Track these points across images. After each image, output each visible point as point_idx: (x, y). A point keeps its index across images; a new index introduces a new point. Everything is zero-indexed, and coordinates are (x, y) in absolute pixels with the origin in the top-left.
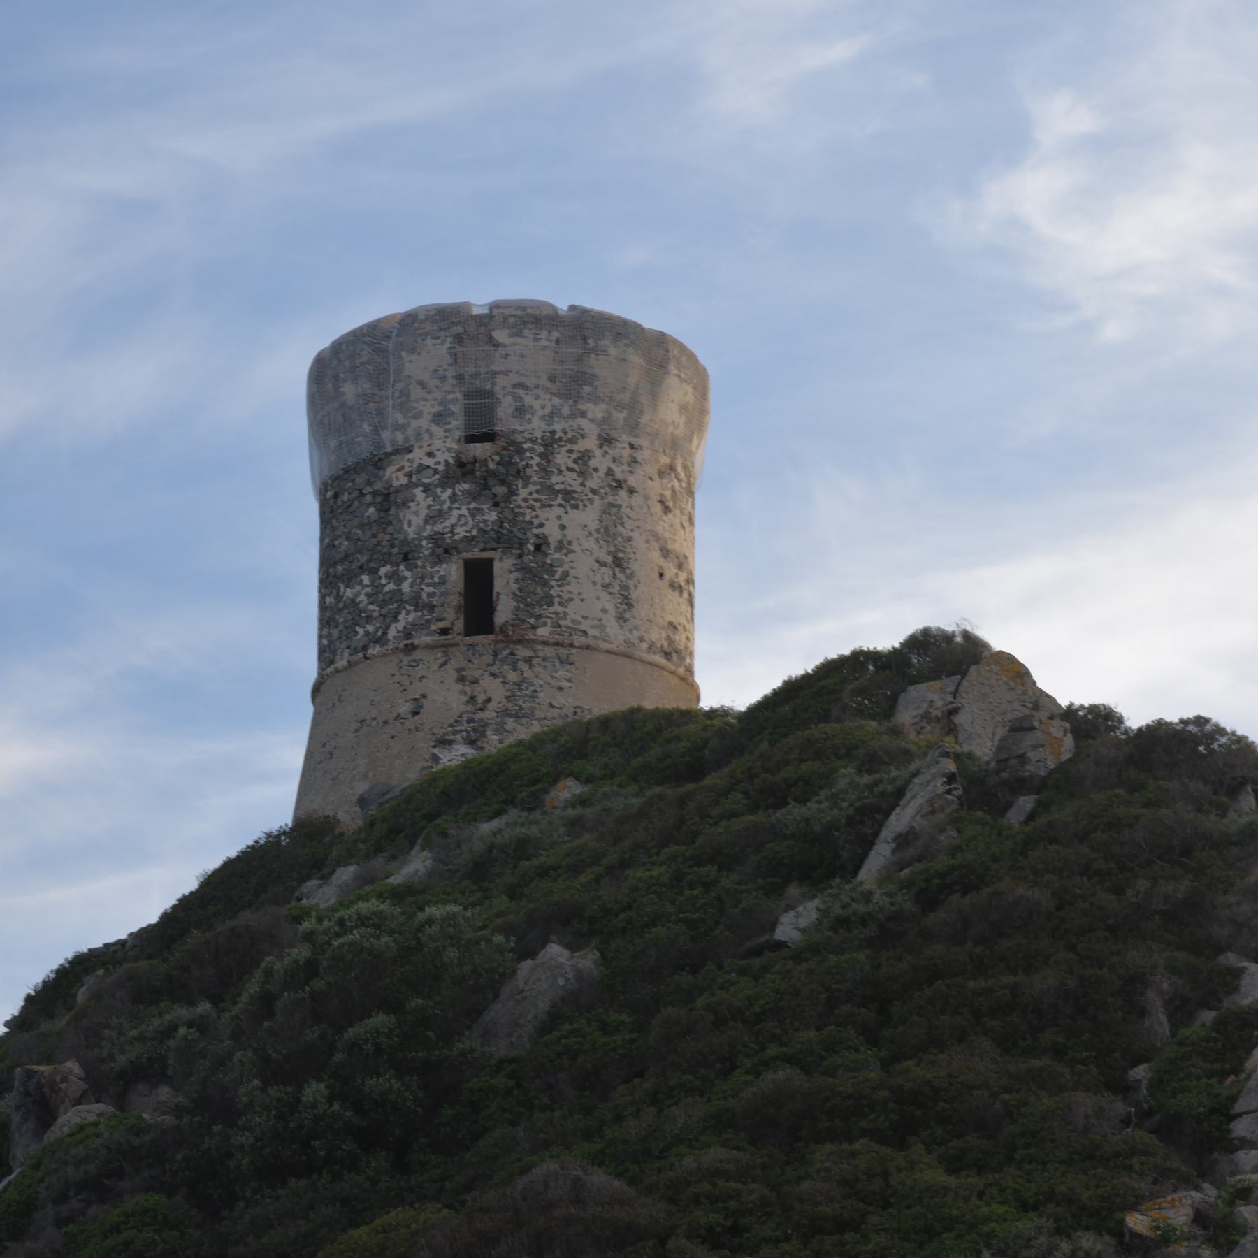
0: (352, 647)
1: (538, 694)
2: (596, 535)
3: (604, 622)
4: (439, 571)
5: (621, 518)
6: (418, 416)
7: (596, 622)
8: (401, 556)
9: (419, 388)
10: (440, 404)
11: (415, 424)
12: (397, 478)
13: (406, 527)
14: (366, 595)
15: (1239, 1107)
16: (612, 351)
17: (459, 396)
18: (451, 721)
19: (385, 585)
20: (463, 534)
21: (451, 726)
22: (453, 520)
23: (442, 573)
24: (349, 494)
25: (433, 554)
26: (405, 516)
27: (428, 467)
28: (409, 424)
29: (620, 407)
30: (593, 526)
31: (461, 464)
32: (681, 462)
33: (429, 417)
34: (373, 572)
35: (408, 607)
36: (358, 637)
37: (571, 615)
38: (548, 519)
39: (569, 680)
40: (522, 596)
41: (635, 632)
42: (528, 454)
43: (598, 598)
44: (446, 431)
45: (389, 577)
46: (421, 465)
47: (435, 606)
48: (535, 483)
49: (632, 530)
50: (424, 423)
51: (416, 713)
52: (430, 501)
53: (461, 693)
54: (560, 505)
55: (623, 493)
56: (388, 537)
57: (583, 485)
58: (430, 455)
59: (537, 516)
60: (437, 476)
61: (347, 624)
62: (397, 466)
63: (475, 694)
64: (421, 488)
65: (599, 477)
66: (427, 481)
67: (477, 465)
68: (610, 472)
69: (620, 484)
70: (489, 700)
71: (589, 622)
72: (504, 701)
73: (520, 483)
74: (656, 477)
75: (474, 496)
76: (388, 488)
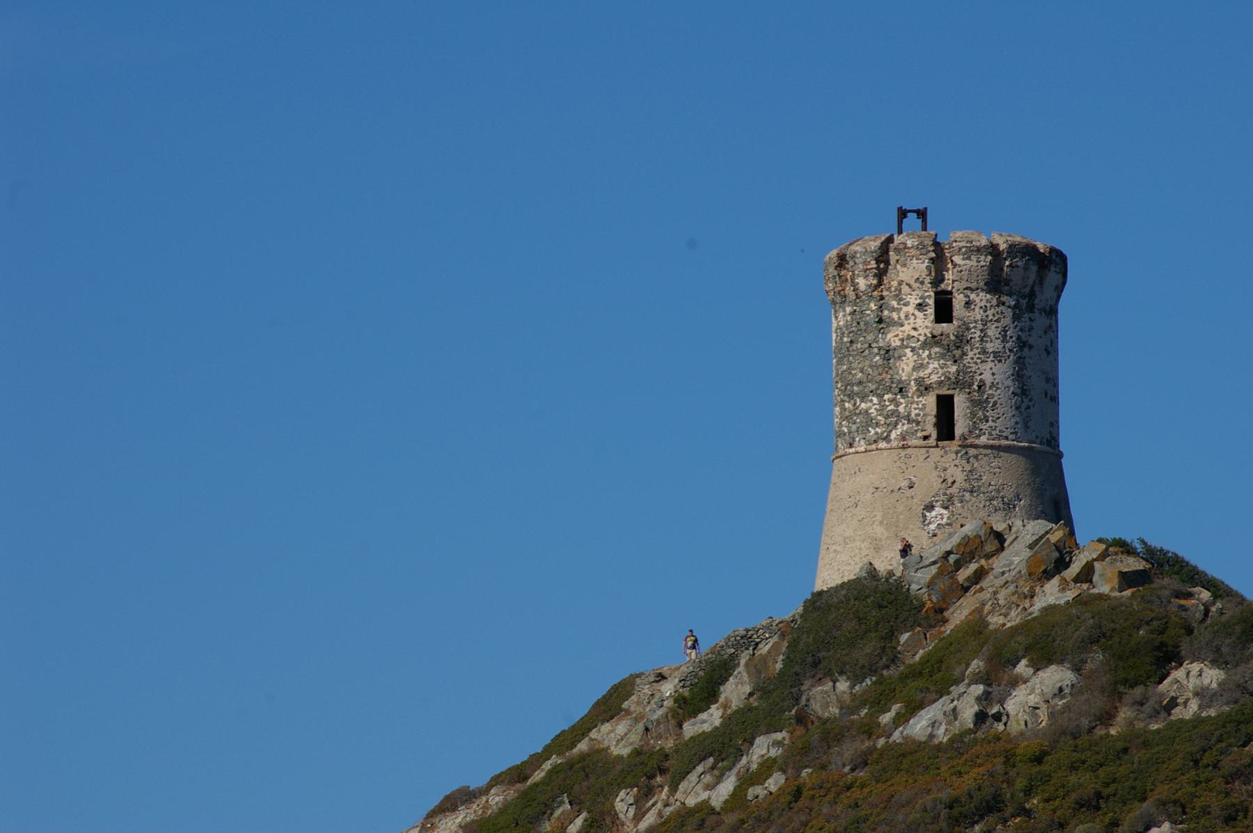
0: (867, 439)
1: (983, 478)
4: (921, 401)
5: (1025, 365)
6: (906, 304)
9: (907, 287)
10: (920, 298)
11: (905, 309)
12: (895, 342)
13: (900, 372)
14: (875, 409)
17: (932, 294)
18: (933, 494)
19: (888, 406)
20: (936, 379)
21: (934, 497)
22: (929, 371)
23: (924, 402)
24: (862, 344)
25: (918, 390)
26: (899, 365)
27: (913, 337)
28: (901, 309)
35: (903, 421)
36: (871, 434)
38: (985, 370)
42: (973, 330)
44: (924, 315)
45: (891, 401)
46: (909, 335)
47: (920, 422)
48: (977, 348)
50: (911, 309)
52: (915, 357)
53: (938, 477)
55: (1026, 350)
58: (915, 329)
60: (920, 343)
61: (862, 424)
62: (895, 334)
63: (946, 478)
64: (910, 349)
66: (913, 345)
70: (954, 482)
72: (964, 482)
75: (943, 356)
76: (889, 346)
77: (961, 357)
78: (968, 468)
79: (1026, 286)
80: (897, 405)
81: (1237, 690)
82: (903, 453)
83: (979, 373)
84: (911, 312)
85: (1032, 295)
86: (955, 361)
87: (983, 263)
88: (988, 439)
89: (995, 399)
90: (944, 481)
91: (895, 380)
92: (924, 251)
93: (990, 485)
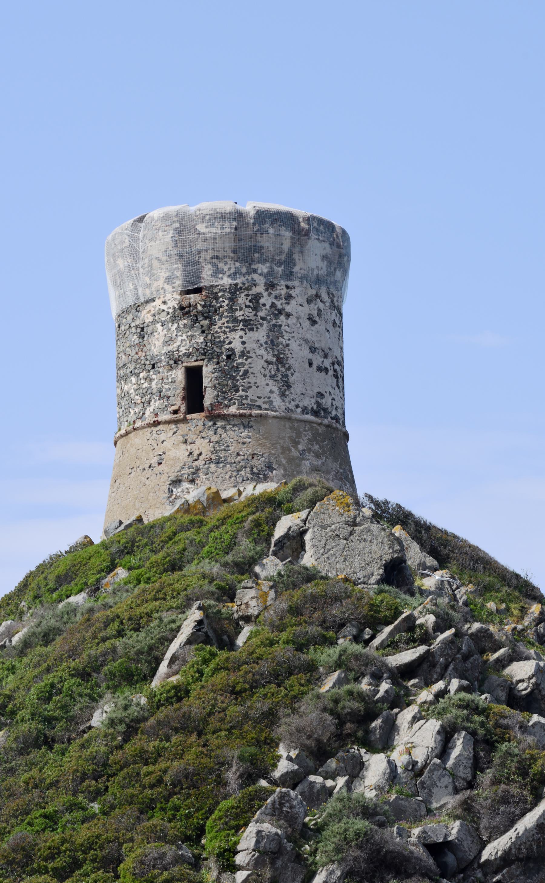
1: (230, 448)
2: (265, 346)
3: (271, 399)
7: (266, 399)
8: (151, 366)
11: (156, 284)
12: (148, 318)
13: (153, 348)
15: (239, 847)
16: (271, 231)
17: (180, 265)
20: (184, 351)
22: (178, 343)
23: (173, 376)
27: (164, 310)
29: (279, 263)
30: (263, 340)
31: (182, 308)
32: (325, 291)
33: (164, 279)
34: (137, 375)
37: (250, 397)
38: (234, 339)
39: (249, 438)
40: (220, 387)
41: (292, 402)
42: (221, 299)
43: (267, 385)
44: (173, 288)
46: (160, 309)
49: (289, 340)
50: (161, 283)
51: (160, 464)
54: (241, 329)
55: (282, 317)
56: (144, 354)
57: (256, 315)
58: (164, 303)
59: (227, 338)
60: (169, 316)
65: (266, 309)
66: (163, 319)
67: (192, 308)
68: (273, 305)
69: (280, 312)
70: (200, 454)
71: (262, 400)
72: (210, 454)
73: (217, 318)
74: (305, 304)
77: (209, 327)
78: (215, 438)
79: (281, 253)
80: (151, 380)
81: (539, 671)
82: (155, 429)
83: (227, 342)
84: (161, 286)
85: (289, 262)
86: (203, 332)
87: (227, 230)
88: (238, 409)
89: (246, 367)
90: (191, 453)
91: (148, 357)
92: (168, 223)
93: (238, 454)
